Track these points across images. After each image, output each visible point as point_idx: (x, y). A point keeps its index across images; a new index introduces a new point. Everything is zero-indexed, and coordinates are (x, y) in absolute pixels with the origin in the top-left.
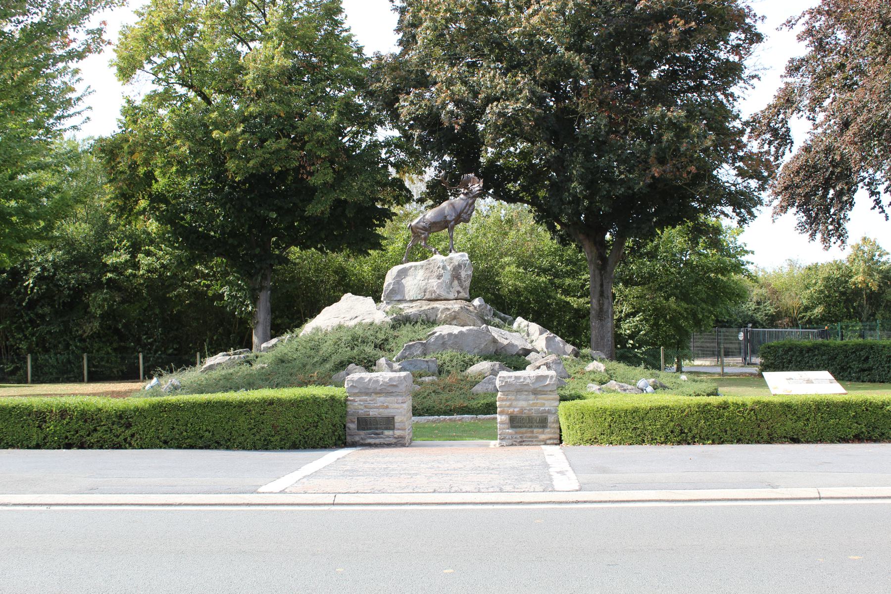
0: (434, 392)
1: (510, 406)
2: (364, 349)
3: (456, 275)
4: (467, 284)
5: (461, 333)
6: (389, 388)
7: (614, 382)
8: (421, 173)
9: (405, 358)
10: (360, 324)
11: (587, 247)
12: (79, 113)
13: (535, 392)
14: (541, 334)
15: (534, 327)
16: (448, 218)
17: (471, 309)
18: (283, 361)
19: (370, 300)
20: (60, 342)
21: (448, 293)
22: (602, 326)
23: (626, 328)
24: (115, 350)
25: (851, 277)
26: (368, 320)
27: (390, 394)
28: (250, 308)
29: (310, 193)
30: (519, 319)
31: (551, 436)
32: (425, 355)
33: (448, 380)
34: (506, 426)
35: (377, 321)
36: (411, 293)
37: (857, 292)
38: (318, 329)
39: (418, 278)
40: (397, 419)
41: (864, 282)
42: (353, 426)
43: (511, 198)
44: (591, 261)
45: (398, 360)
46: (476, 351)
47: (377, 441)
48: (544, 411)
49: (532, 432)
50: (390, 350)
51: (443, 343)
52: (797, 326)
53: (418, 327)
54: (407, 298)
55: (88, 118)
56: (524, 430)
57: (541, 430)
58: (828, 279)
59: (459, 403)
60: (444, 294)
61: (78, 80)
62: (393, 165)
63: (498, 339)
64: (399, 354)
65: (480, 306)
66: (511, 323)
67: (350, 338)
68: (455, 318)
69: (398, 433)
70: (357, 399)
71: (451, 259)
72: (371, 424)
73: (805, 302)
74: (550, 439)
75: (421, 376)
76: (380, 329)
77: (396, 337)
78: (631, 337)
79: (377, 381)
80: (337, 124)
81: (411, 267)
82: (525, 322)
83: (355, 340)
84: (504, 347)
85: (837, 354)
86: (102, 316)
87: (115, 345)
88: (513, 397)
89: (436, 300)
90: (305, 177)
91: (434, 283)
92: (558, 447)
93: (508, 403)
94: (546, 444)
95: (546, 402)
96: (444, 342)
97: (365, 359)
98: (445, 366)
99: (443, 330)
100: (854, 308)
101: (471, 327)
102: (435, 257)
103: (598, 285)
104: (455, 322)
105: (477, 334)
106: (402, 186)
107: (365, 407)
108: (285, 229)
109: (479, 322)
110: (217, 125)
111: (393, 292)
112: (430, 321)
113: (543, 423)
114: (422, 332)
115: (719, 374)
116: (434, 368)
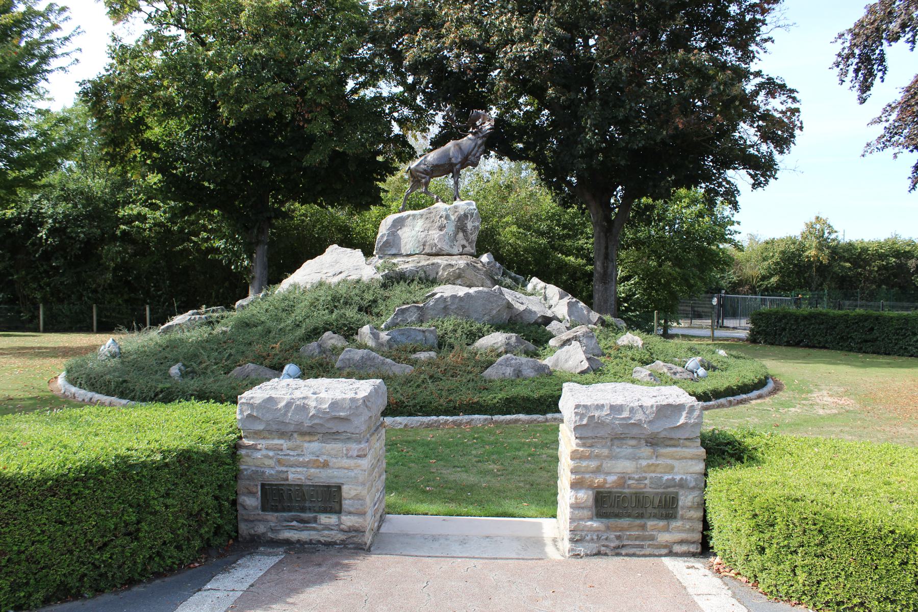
0: (431, 377)
1: (598, 470)
2: (346, 311)
3: (461, 226)
4: (474, 237)
5: (468, 295)
6: (329, 425)
7: (662, 364)
8: (425, 130)
9: (396, 325)
10: (345, 281)
12: (67, 54)
13: (654, 441)
14: (561, 298)
15: (553, 291)
16: (453, 160)
17: (479, 266)
18: (247, 325)
19: (358, 253)
20: (73, 293)
21: (451, 247)
22: (606, 289)
23: (622, 290)
24: (126, 301)
25: (804, 252)
26: (354, 277)
27: (332, 436)
28: (246, 263)
29: (307, 143)
30: (535, 280)
31: (683, 536)
32: (422, 322)
33: (451, 358)
34: (587, 513)
35: (365, 279)
36: (408, 247)
37: (810, 264)
38: (295, 286)
39: (417, 229)
40: (348, 491)
42: (251, 502)
43: (515, 156)
44: (597, 222)
45: (387, 328)
46: (486, 318)
47: (304, 536)
48: (672, 483)
49: (643, 527)
50: (378, 315)
51: (446, 308)
52: (755, 293)
53: (414, 286)
54: (403, 252)
55: (77, 60)
56: (624, 522)
57: (662, 523)
58: (783, 252)
59: (468, 396)
60: (446, 248)
61: (66, 19)
62: (397, 121)
63: (513, 303)
64: (389, 320)
65: (488, 263)
66: (525, 285)
67: (329, 298)
68: (459, 276)
69: (348, 521)
70: (262, 444)
71: (456, 207)
72: (290, 499)
73: (763, 272)
74: (681, 542)
75: (414, 351)
76: (369, 288)
77: (385, 299)
78: (625, 300)
79: (304, 408)
80: (339, 70)
81: (409, 216)
82: (542, 284)
83: (336, 301)
84: (521, 314)
85: (837, 324)
86: (115, 270)
87: (126, 297)
88: (605, 452)
89: (437, 255)
90: (301, 124)
91: (435, 235)
92: (698, 563)
93: (593, 464)
94: (671, 554)
95: (676, 463)
96: (446, 307)
97: (345, 325)
98: (446, 337)
99: (445, 291)
100: (805, 278)
101: (481, 288)
102: (436, 205)
103: (603, 246)
104: (459, 281)
106: (405, 143)
107: (279, 462)
108: (283, 181)
109: (489, 282)
110: (211, 65)
111: (387, 244)
112: (429, 279)
113: (666, 507)
114: (419, 293)
115: (708, 337)
116: (432, 340)
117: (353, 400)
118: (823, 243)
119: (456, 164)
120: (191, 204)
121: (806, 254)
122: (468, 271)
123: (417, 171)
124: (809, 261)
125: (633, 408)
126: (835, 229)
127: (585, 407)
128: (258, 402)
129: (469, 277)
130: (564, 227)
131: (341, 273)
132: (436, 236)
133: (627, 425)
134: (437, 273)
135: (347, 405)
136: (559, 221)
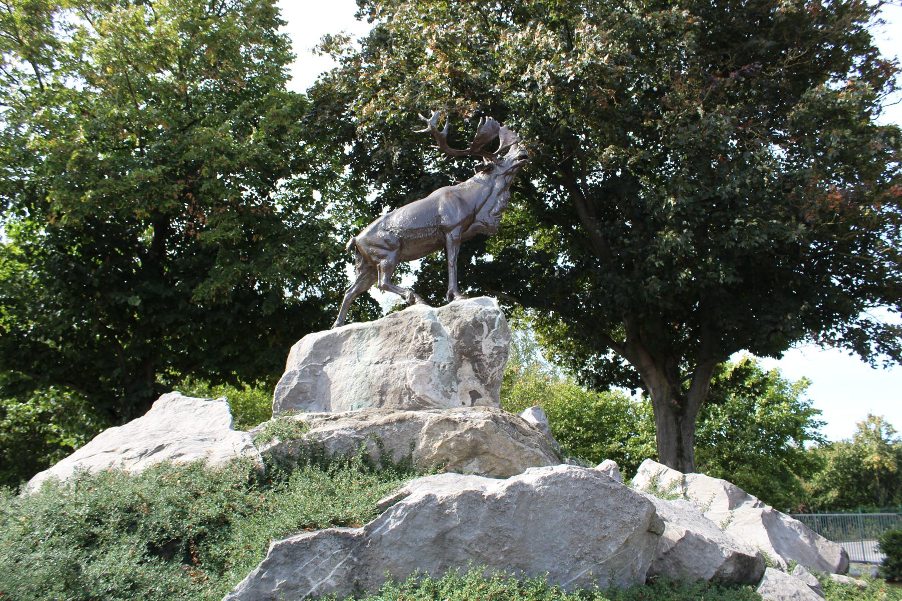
10: (161, 468)
11: (653, 379)
14: (734, 504)
16: (445, 221)
25: (864, 457)
26: (189, 458)
36: (345, 399)
41: (880, 462)
51: (443, 540)
81: (349, 333)
103: (674, 437)
104: (474, 464)
105: (589, 500)
114: (356, 495)
118: (884, 449)
119: (449, 230)
121: (867, 459)
122: (497, 438)
124: (871, 468)
126: (895, 428)
129: (501, 453)
130: (587, 427)
131: (160, 448)
132: (411, 370)
134: (413, 446)
136: (579, 419)
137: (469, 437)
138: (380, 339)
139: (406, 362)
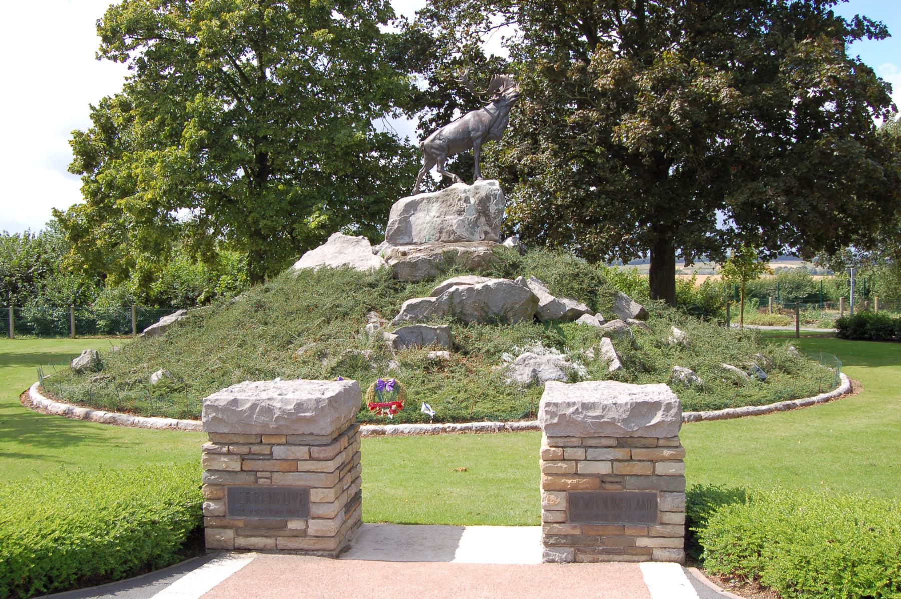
36: (422, 235)
39: (433, 214)
40: (315, 496)
60: (465, 234)
71: (477, 188)
79: (269, 410)
81: (423, 199)
91: (453, 220)
101: (501, 280)
102: (453, 186)
117: (318, 401)
120: (592, 189)
123: (432, 147)
125: (606, 406)
127: (556, 405)
128: (222, 404)
132: (455, 221)
133: (599, 424)
135: (313, 405)
137: (476, 259)
138: (439, 204)
139: (452, 217)
